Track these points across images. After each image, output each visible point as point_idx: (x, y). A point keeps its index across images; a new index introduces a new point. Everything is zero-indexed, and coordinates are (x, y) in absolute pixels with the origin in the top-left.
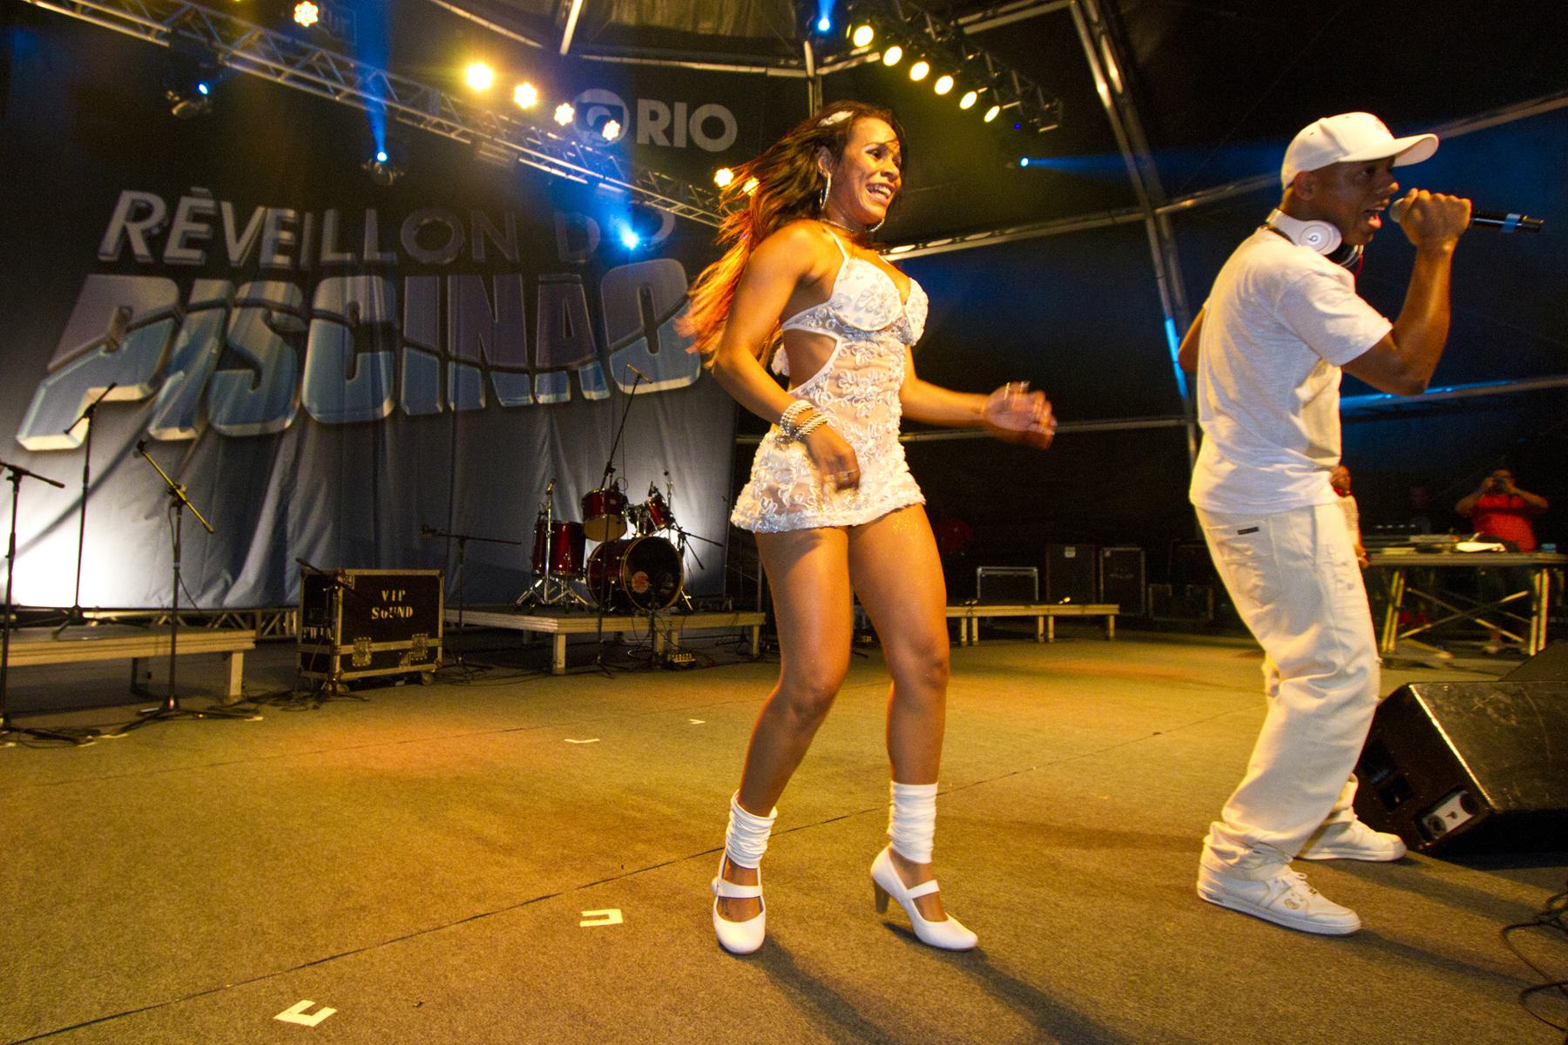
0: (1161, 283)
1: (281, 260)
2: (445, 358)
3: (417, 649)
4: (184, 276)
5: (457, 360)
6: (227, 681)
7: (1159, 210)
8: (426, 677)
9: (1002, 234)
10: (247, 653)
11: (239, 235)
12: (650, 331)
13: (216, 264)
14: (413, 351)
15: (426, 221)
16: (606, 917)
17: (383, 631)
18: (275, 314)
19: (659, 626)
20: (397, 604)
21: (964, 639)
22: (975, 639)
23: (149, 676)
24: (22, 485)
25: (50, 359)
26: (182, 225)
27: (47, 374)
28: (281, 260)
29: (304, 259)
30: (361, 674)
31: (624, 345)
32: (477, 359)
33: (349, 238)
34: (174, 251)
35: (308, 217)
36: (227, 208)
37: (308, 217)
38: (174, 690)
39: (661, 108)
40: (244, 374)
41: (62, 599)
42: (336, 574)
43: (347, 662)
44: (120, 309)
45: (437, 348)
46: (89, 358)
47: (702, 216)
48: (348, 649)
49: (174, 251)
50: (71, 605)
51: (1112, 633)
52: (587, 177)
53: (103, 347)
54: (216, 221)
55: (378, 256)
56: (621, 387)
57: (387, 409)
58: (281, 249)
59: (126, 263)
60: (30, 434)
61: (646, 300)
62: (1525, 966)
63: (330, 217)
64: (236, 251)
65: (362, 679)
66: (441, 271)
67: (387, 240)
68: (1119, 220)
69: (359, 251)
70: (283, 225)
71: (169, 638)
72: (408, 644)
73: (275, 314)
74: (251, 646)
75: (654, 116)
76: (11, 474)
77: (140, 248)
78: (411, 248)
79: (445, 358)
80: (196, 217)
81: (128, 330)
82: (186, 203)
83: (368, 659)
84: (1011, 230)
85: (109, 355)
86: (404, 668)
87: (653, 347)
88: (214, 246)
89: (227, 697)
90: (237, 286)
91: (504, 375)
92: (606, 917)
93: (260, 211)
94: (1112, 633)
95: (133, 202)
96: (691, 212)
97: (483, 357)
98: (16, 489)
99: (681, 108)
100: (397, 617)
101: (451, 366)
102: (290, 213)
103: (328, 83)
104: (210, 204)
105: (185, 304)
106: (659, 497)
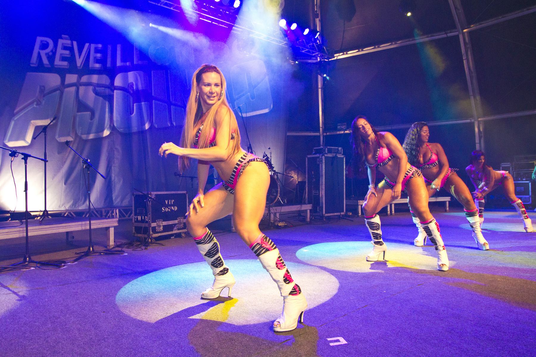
0: (465, 62)
1: (98, 66)
2: (170, 104)
3: (180, 223)
4: (62, 72)
5: (175, 105)
6: (109, 239)
7: (465, 31)
8: (183, 235)
9: (396, 44)
10: (115, 228)
13: (73, 69)
14: (157, 102)
17: (167, 217)
18: (97, 89)
19: (272, 211)
20: (171, 205)
21: (389, 213)
22: (393, 212)
23: (73, 237)
24: (28, 161)
26: (60, 51)
27: (14, 115)
29: (109, 65)
30: (160, 234)
35: (110, 47)
36: (75, 43)
37: (110, 47)
38: (91, 243)
40: (88, 113)
41: (21, 208)
42: (149, 194)
43: (154, 229)
44: (40, 87)
46: (30, 108)
48: (154, 225)
49: (58, 62)
50: (23, 210)
51: (448, 209)
53: (35, 103)
54: (71, 49)
55: (140, 62)
57: (147, 126)
58: (97, 61)
59: (40, 68)
60: (9, 141)
62: (9, 287)
64: (79, 62)
65: (159, 236)
70: (97, 51)
71: (88, 222)
72: (176, 222)
74: (116, 224)
76: (23, 156)
77: (45, 61)
79: (170, 104)
80: (65, 48)
81: (44, 96)
82: (61, 42)
83: (161, 228)
84: (400, 42)
85: (37, 106)
86: (175, 232)
88: (71, 60)
89: (109, 246)
93: (87, 45)
94: (448, 209)
98: (26, 163)
100: (172, 210)
101: (172, 107)
102: (100, 46)
104: (69, 42)
105: (64, 85)
106: (268, 158)
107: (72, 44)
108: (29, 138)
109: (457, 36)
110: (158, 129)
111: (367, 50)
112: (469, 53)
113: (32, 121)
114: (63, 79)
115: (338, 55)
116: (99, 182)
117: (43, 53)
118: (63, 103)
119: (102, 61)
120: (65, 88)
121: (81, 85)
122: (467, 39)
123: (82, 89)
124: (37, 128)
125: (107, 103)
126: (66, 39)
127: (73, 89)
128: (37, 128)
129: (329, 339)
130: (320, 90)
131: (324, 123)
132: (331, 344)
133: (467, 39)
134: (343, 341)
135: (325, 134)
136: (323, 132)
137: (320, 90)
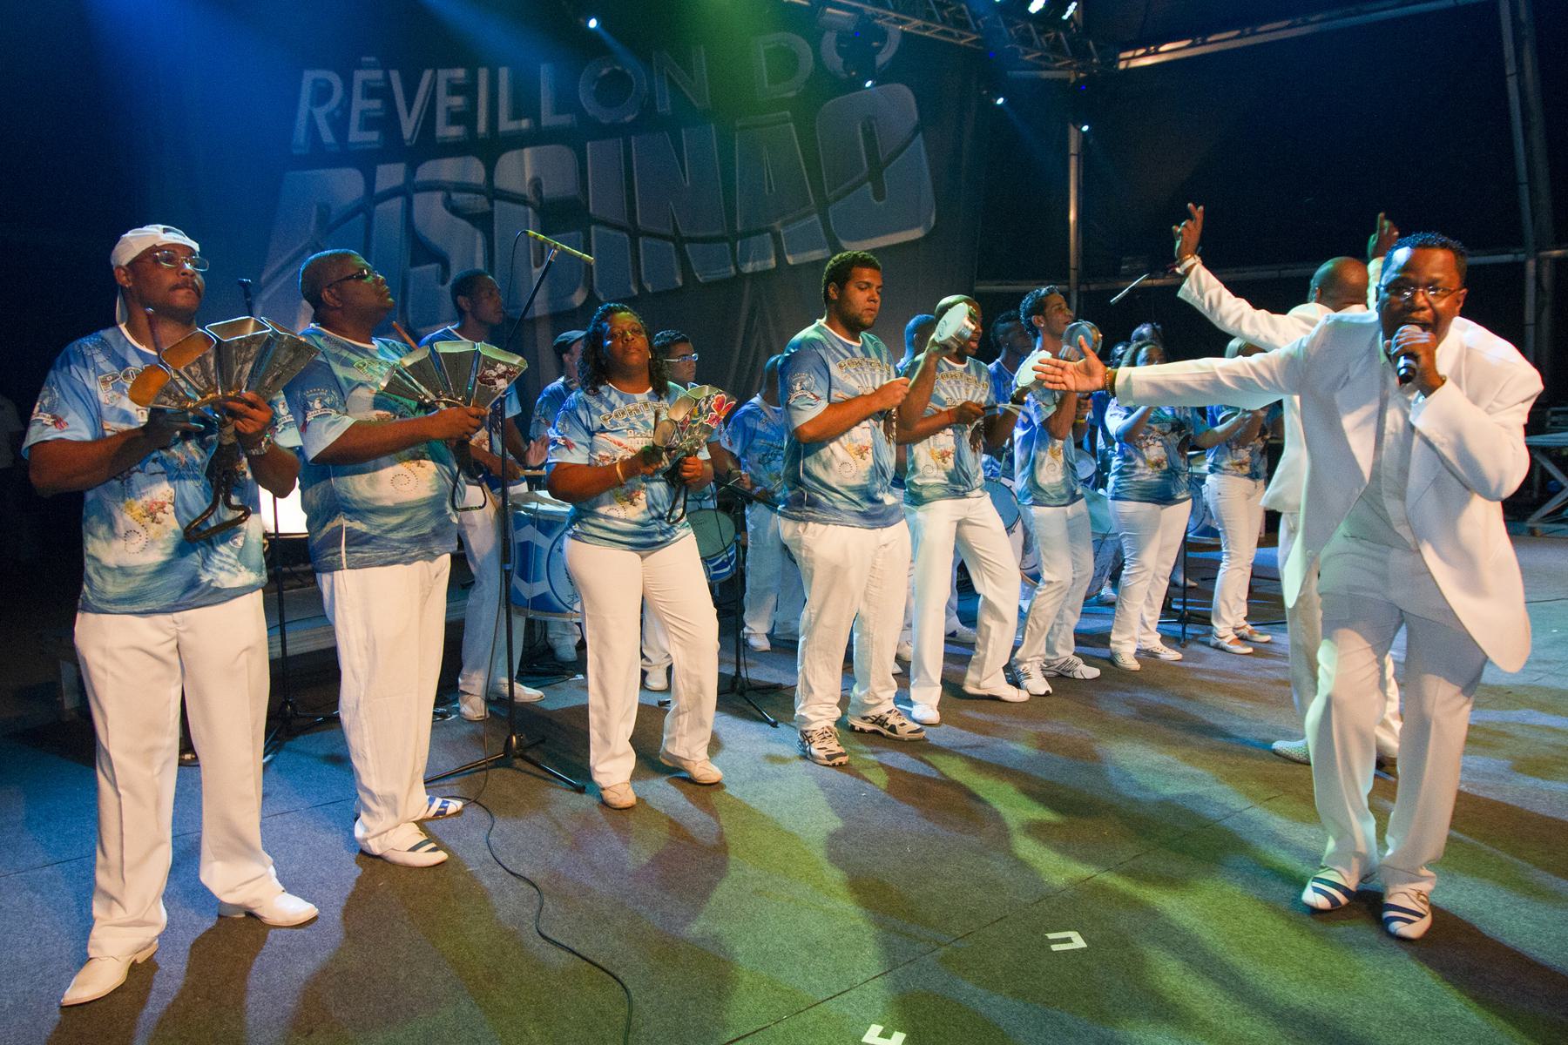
1: (455, 131)
2: (635, 234)
4: (366, 162)
11: (409, 110)
12: (876, 175)
14: (602, 229)
15: (605, 72)
16: (1068, 940)
18: (454, 196)
26: (359, 104)
28: (455, 131)
29: (482, 127)
31: (849, 191)
32: (669, 231)
34: (356, 135)
35: (483, 74)
36: (395, 75)
45: (624, 221)
47: (943, 32)
49: (356, 135)
54: (385, 93)
58: (454, 118)
59: (321, 157)
64: (409, 126)
69: (535, 116)
70: (454, 89)
73: (454, 196)
77: (327, 136)
80: (370, 92)
84: (1318, 17)
87: (879, 194)
88: (387, 122)
90: (412, 169)
91: (700, 246)
92: (1068, 940)
93: (427, 75)
95: (315, 81)
96: (927, 28)
97: (676, 228)
102: (460, 73)
105: (372, 198)
107: (387, 79)
111: (1221, 41)
114: (370, 182)
115: (1130, 54)
116: (981, 784)
117: (320, 113)
119: (464, 117)
120: (376, 203)
121: (417, 191)
123: (419, 199)
125: (479, 235)
126: (370, 66)
127: (396, 204)
130: (1073, 161)
131: (1085, 255)
133: (1523, 16)
134: (1078, 942)
135: (1083, 288)
136: (1079, 284)
137: (1073, 161)
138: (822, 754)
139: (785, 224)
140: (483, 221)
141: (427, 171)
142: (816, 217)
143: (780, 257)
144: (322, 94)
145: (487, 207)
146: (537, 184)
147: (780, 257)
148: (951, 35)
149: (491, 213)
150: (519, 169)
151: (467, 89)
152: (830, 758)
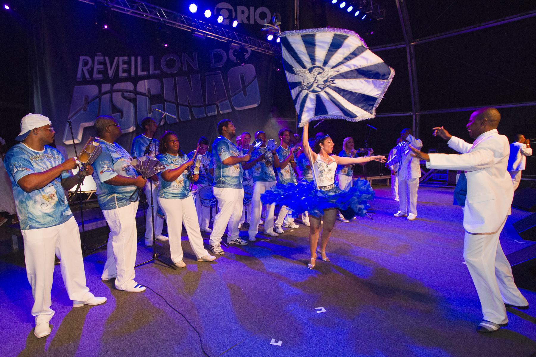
1: (125, 75)
2: (178, 105)
4: (99, 83)
13: (107, 80)
18: (125, 93)
25: (68, 115)
26: (97, 67)
28: (125, 75)
29: (133, 73)
32: (187, 104)
33: (145, 67)
34: (96, 76)
35: (133, 58)
36: (107, 58)
37: (133, 58)
39: (245, 9)
45: (175, 101)
49: (96, 76)
52: (227, 40)
54: (104, 63)
56: (236, 108)
58: (125, 71)
59: (85, 82)
60: (66, 140)
61: (489, 167)
63: (139, 58)
64: (111, 73)
66: (172, 75)
67: (157, 66)
68: (398, 47)
69: (148, 71)
70: (124, 63)
73: (125, 93)
75: (243, 12)
77: (87, 76)
78: (165, 69)
80: (100, 63)
82: (96, 58)
87: (245, 94)
88: (104, 72)
90: (112, 85)
93: (116, 58)
96: (258, 49)
99: (252, 9)
102: (126, 58)
103: (125, 9)
104: (102, 58)
105: (101, 94)
108: (80, 137)
109: (404, 49)
110: (184, 122)
112: (413, 62)
113: (81, 124)
118: (101, 109)
119: (128, 71)
121: (113, 92)
122: (412, 51)
123: (115, 94)
124: (86, 129)
126: (100, 56)
127: (108, 95)
128: (86, 129)
129: (316, 309)
132: (318, 312)
133: (412, 51)
138: (217, 252)
139: (220, 102)
140: (133, 101)
141: (117, 86)
142: (228, 100)
143: (218, 112)
144: (86, 64)
145: (135, 97)
146: (149, 90)
147: (218, 112)
148: (265, 51)
149: (136, 99)
150: (144, 86)
151: (129, 63)
152: (219, 253)
